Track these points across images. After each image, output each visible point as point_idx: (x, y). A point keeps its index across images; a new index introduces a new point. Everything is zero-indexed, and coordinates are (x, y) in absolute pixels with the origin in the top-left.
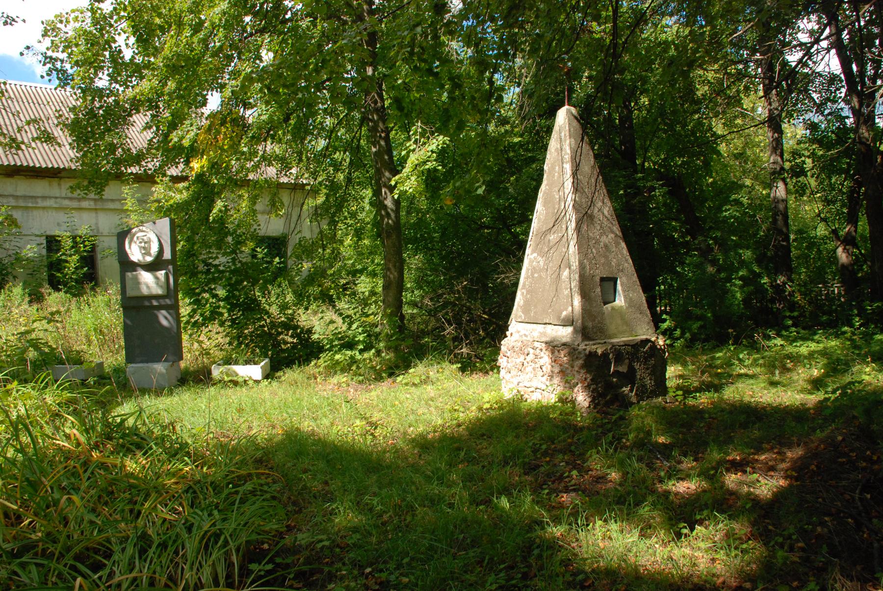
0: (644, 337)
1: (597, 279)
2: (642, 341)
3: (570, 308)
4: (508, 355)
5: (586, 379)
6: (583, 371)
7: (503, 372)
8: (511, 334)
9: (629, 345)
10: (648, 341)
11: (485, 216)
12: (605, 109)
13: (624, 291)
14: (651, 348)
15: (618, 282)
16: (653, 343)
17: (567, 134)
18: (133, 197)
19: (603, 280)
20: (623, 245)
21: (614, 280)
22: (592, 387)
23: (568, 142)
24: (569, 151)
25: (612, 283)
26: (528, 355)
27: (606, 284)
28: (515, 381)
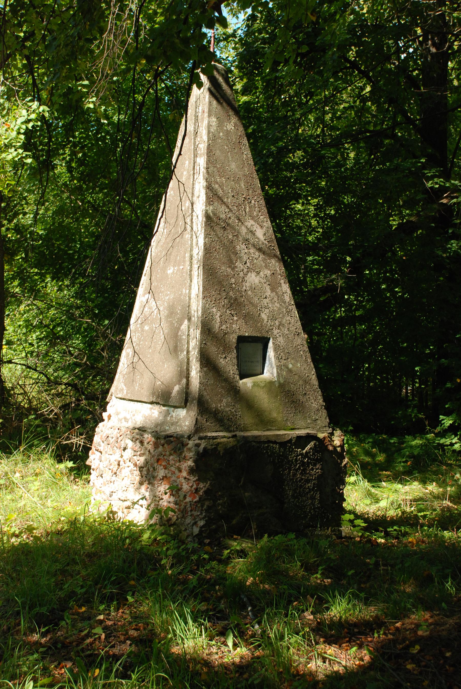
0: (302, 432)
1: (233, 339)
2: (299, 438)
3: (184, 381)
4: (101, 449)
5: (197, 490)
6: (193, 478)
7: (93, 477)
8: (109, 417)
9: (275, 442)
10: (309, 438)
11: (22, 218)
12: (150, 43)
13: (278, 358)
14: (314, 449)
15: (271, 344)
16: (321, 441)
17: (206, 110)
18: (60, 211)
19: (241, 339)
20: (286, 288)
21: (264, 342)
22: (207, 503)
23: (206, 122)
24: (205, 138)
25: (260, 346)
26: (125, 449)
27: (249, 348)
28: (107, 490)
